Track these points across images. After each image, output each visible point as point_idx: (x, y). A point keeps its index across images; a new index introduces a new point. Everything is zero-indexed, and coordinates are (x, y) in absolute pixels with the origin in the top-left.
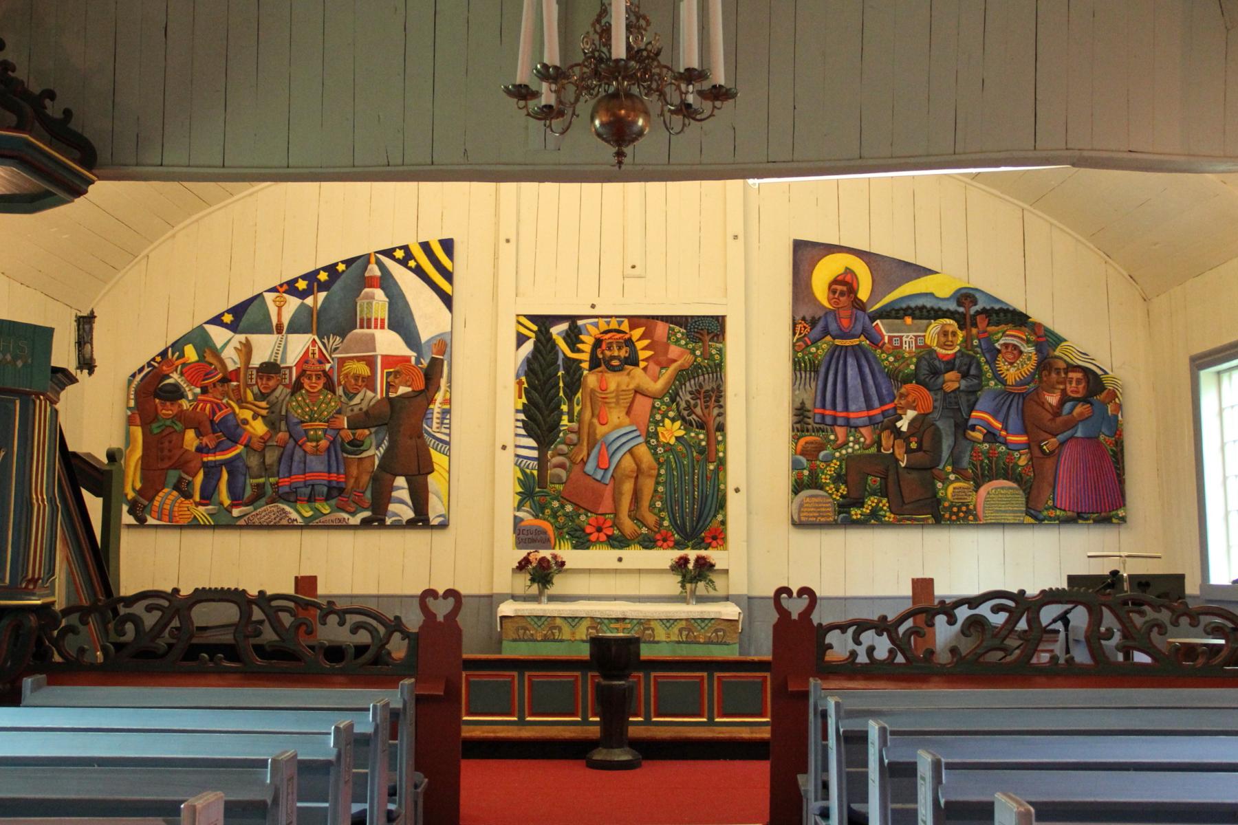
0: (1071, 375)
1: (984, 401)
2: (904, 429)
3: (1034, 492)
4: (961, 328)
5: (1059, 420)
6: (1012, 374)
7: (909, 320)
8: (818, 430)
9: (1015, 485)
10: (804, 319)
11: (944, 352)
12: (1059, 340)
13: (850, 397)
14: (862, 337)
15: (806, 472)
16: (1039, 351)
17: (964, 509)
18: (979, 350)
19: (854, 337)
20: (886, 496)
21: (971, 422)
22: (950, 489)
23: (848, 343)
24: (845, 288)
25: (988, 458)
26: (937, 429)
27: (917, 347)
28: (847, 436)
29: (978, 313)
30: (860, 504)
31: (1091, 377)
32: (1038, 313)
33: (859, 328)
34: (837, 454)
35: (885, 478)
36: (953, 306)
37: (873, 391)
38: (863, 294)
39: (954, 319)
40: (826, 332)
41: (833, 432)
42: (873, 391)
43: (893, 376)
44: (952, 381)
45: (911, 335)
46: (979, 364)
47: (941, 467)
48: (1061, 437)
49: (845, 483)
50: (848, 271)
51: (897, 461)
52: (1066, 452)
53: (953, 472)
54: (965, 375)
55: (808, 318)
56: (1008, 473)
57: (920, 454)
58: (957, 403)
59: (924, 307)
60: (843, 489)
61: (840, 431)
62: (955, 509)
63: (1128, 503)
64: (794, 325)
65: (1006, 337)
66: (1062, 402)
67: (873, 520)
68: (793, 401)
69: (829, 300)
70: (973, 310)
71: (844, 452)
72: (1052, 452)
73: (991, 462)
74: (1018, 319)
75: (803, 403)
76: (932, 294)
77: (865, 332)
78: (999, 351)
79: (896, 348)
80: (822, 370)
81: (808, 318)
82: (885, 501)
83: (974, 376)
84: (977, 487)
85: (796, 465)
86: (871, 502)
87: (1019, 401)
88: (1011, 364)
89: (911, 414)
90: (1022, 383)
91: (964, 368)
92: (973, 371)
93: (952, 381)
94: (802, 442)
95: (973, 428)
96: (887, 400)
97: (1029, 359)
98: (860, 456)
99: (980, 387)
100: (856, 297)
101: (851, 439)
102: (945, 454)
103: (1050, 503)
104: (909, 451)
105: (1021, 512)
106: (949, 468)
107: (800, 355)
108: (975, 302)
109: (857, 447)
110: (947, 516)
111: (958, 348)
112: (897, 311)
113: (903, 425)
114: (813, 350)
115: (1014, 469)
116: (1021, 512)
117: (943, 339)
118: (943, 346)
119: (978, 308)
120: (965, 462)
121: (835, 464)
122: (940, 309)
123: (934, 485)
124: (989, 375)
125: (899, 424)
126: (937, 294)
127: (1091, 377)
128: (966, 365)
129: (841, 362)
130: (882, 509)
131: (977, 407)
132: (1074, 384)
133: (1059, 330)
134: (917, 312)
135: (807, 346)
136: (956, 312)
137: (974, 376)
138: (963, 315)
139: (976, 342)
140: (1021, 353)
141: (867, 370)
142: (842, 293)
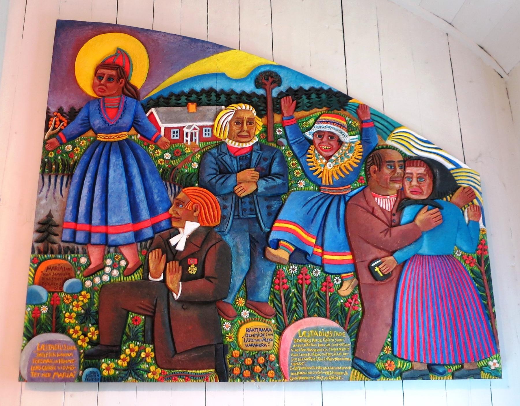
0: (409, 170)
1: (292, 210)
2: (181, 247)
3: (364, 334)
4: (259, 115)
5: (395, 231)
6: (328, 168)
7: (192, 107)
8: (67, 250)
9: (335, 325)
10: (60, 110)
11: (237, 145)
12: (391, 126)
13: (110, 206)
14: (133, 131)
15: (44, 310)
16: (364, 140)
17: (262, 360)
18: (284, 141)
19: (120, 130)
20: (152, 342)
21: (274, 236)
22: (243, 331)
23: (114, 138)
24: (114, 73)
25: (296, 286)
26: (226, 248)
27: (201, 139)
28: (104, 258)
29: (281, 95)
30: (115, 353)
31: (437, 172)
32: (361, 92)
33: (128, 119)
34: (88, 284)
35: (152, 317)
36: (249, 88)
37: (141, 196)
38: (138, 79)
39: (251, 103)
40: (87, 126)
41: (85, 253)
42: (141, 196)
43: (169, 176)
44: (247, 182)
45: (195, 124)
46: (283, 161)
47: (229, 300)
48: (400, 255)
49: (96, 323)
50: (121, 53)
51: (169, 291)
52: (409, 275)
53: (247, 306)
54: (265, 174)
55: (66, 109)
56: (323, 305)
57: (201, 282)
58: (253, 211)
59: (211, 90)
60: (93, 332)
61: (95, 253)
62: (249, 361)
63: (501, 348)
64: (48, 119)
65: (321, 124)
66: (400, 207)
67: (133, 372)
68: (37, 213)
69: (94, 86)
70: (275, 93)
71: (97, 280)
72: (386, 276)
73: (300, 291)
74: (335, 101)
75: (50, 216)
76: (223, 75)
77: (135, 124)
78: (311, 142)
79: (176, 141)
80: (77, 172)
81: (66, 109)
82: (149, 349)
83: (278, 175)
84: (281, 331)
85: (32, 298)
86: (130, 350)
87: (340, 204)
88: (328, 158)
89: (191, 227)
90: (344, 182)
91: (264, 164)
92: (275, 168)
93: (247, 182)
94: (43, 267)
95: (277, 245)
96: (160, 209)
97: (350, 150)
98: (121, 283)
99: (286, 189)
100: (127, 82)
101: (109, 262)
102: (237, 280)
103: (387, 351)
104: (186, 278)
105: (345, 363)
106: (241, 302)
107: (52, 155)
108: (278, 82)
109: (115, 273)
110: (237, 371)
111: (256, 140)
112: (178, 96)
113: (179, 241)
114: (69, 148)
115: (333, 300)
116: (345, 363)
117: (236, 129)
118: (239, 137)
119: (283, 88)
120: (264, 293)
121: (84, 298)
122: (233, 92)
123: (220, 326)
124: (298, 172)
125: (173, 241)
126: (229, 75)
127: (437, 172)
128: (266, 160)
129: (102, 161)
130: (144, 360)
131: (281, 216)
132: (414, 183)
133: (391, 112)
134: (204, 97)
135: (62, 144)
136: (254, 94)
137: (278, 175)
138: (264, 99)
139: (279, 132)
140: (340, 143)
141: (135, 171)
142: (110, 79)
